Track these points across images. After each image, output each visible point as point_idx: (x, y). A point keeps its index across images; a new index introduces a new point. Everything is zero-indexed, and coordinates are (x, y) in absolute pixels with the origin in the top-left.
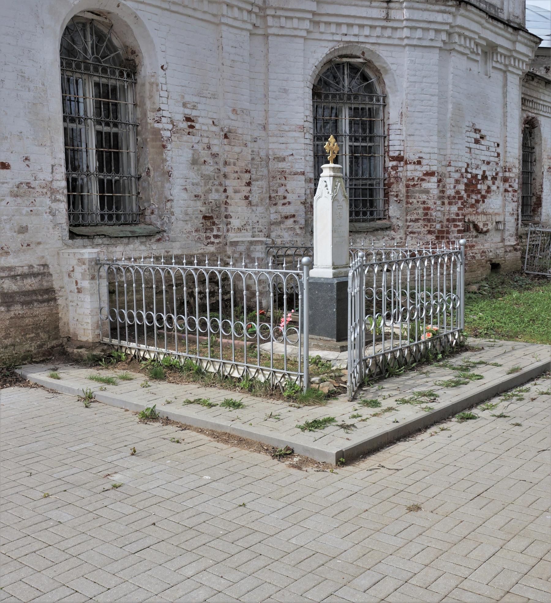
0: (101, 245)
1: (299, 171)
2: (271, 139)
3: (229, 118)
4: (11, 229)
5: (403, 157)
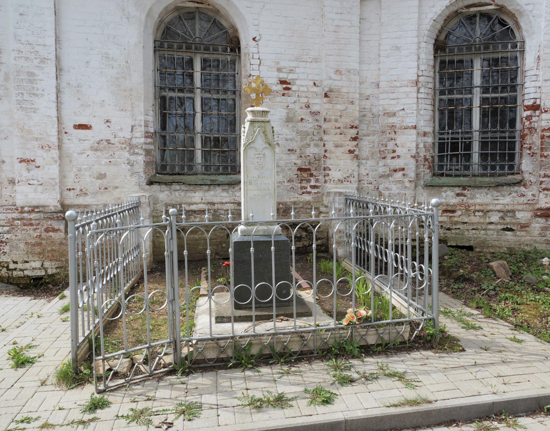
0: (179, 190)
1: (410, 125)
2: (382, 96)
3: (331, 79)
4: (90, 176)
5: (539, 106)
